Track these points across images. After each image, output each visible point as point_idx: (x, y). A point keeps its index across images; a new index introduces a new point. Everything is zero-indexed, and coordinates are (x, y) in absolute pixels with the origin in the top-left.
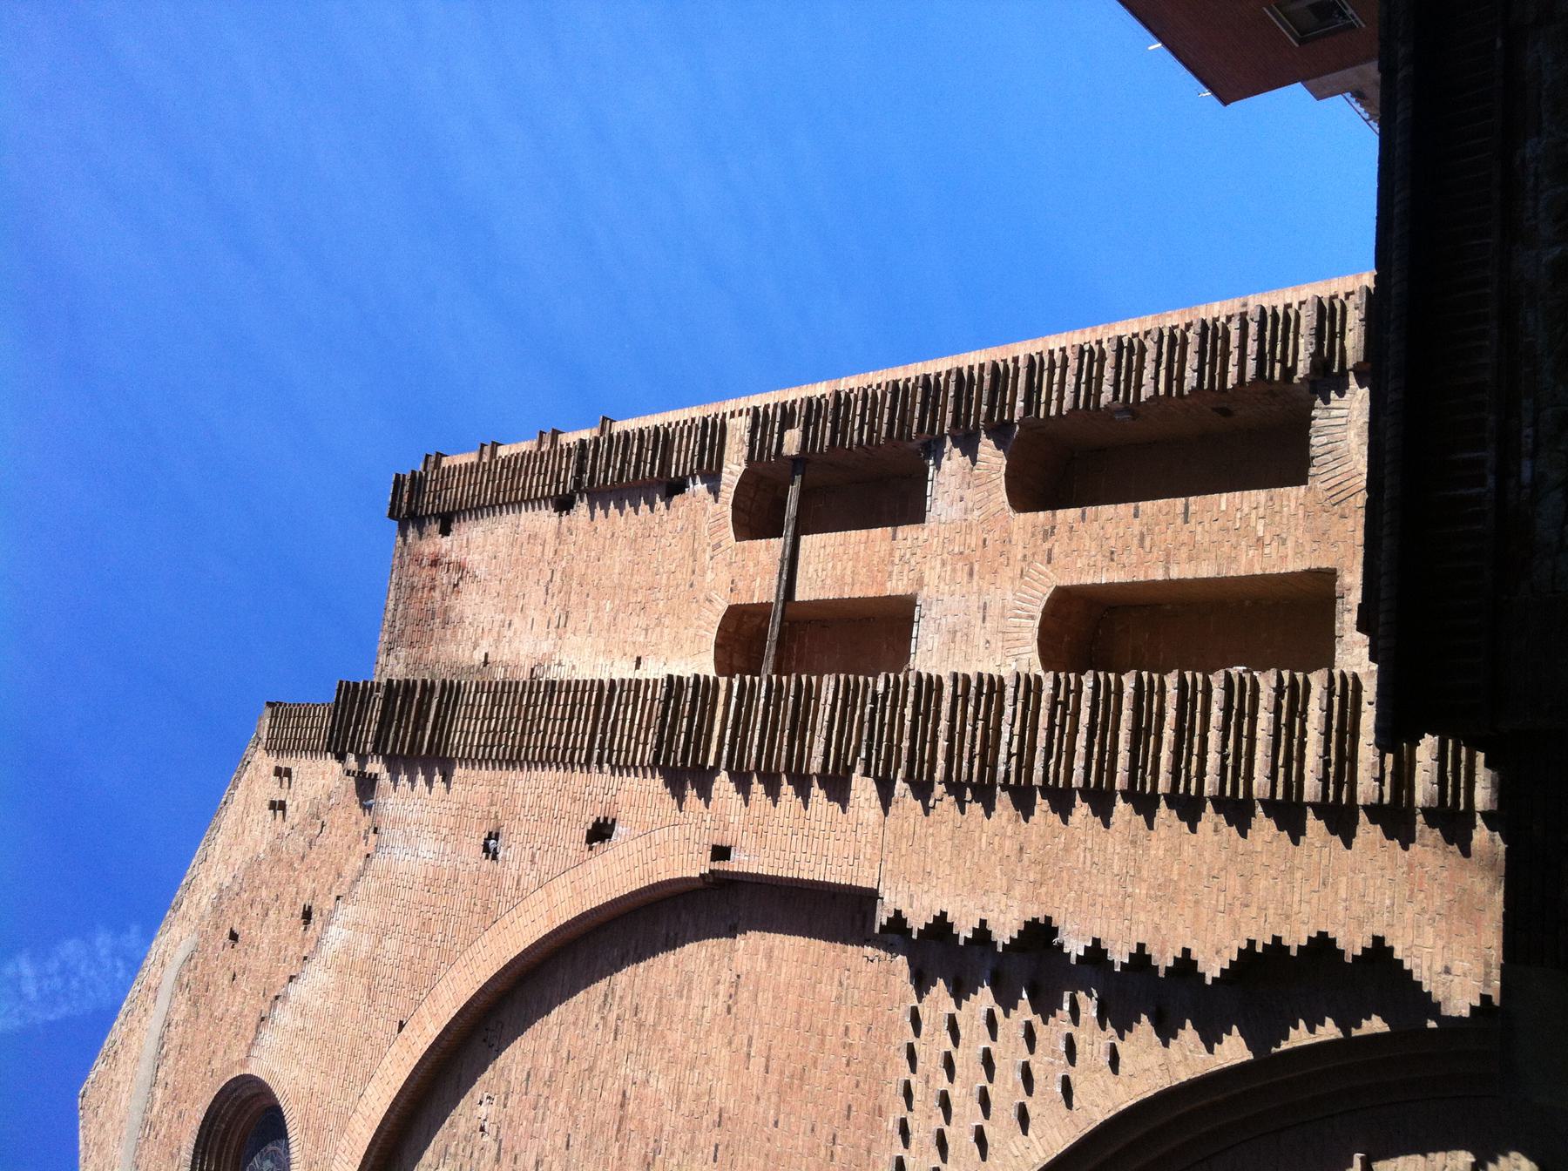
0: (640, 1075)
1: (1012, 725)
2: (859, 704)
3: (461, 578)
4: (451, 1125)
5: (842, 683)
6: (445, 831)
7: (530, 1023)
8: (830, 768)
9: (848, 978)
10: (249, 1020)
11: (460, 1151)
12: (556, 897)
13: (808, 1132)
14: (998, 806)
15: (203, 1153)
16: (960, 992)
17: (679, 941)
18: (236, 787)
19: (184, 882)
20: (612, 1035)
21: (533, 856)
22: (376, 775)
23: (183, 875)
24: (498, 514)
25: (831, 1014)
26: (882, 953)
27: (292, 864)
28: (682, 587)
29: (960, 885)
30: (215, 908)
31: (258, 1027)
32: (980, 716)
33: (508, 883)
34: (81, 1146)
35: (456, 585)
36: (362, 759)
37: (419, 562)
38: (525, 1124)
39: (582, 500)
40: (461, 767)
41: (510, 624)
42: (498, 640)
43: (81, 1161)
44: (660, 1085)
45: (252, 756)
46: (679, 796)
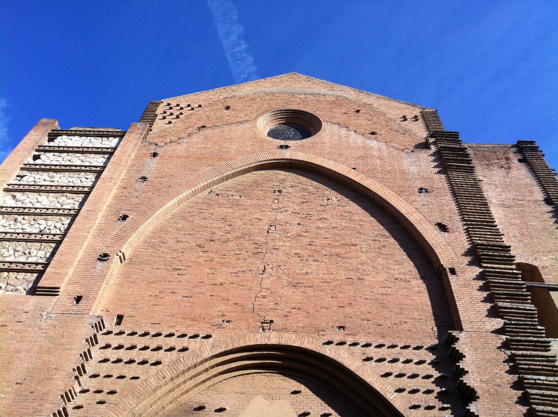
0: (364, 250)
1: (547, 380)
2: (527, 319)
3: (505, 168)
4: (326, 189)
5: (534, 312)
6: (421, 174)
7: (367, 210)
8: (502, 310)
9: (423, 322)
10: (335, 120)
11: (319, 193)
12: (415, 215)
13: (368, 311)
14: (511, 376)
15: (294, 113)
16: (433, 364)
17: (412, 259)
18: (405, 104)
19: (369, 93)
20: (373, 239)
21: (425, 205)
22: (431, 149)
23: (372, 92)
24: (534, 178)
25: (409, 316)
26: (436, 334)
27: (388, 126)
28: (536, 248)
29: (477, 362)
30: (364, 104)
31: (337, 123)
32: (544, 367)
33: (413, 198)
34: (280, 76)
35: (502, 167)
36: (434, 143)
37: (505, 153)
38: (335, 213)
39: (553, 208)
40: (445, 177)
41: (496, 187)
42: (489, 184)
43: (276, 77)
44: (364, 257)
45: (417, 107)
46: (467, 254)
